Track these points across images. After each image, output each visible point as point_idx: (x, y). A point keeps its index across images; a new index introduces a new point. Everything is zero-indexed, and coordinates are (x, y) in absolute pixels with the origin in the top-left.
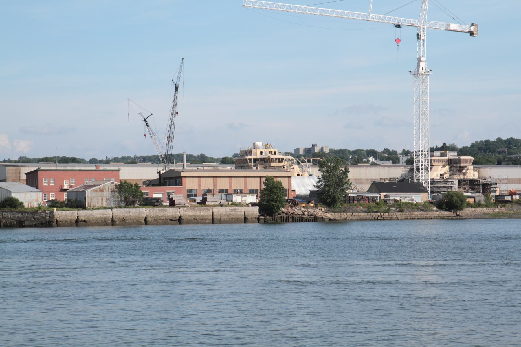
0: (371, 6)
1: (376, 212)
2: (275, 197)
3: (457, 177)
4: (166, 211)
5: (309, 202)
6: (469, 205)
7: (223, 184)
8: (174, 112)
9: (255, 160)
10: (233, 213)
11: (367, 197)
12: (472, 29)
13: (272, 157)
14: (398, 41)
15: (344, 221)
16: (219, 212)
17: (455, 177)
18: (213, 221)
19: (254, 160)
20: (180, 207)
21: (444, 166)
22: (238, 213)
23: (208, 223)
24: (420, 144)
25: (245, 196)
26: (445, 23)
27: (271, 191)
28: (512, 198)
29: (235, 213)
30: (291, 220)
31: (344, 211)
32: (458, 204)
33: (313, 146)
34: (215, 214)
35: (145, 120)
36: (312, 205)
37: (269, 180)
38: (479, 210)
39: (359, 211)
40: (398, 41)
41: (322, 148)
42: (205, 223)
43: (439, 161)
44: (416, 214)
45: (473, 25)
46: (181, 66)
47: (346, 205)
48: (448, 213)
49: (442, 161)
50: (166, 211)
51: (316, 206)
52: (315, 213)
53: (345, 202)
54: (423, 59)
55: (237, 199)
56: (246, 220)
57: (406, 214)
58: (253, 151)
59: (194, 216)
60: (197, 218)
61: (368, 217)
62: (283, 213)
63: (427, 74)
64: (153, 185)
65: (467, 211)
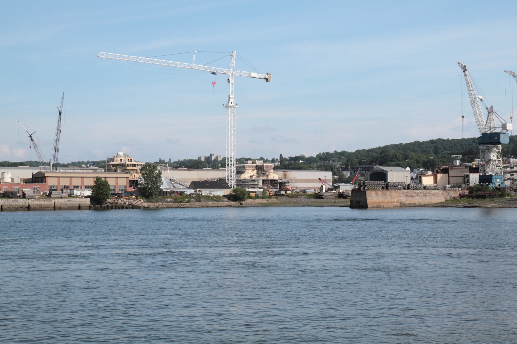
0: (194, 59)
1: (181, 202)
2: (102, 191)
3: (262, 178)
4: (17, 201)
5: (132, 195)
6: (250, 197)
7: (65, 182)
8: (59, 131)
9: (116, 165)
10: (70, 203)
11: (177, 192)
12: (267, 77)
13: (128, 163)
14: (214, 84)
15: (156, 209)
16: (59, 202)
17: (261, 178)
18: (55, 208)
19: (115, 165)
20: (29, 199)
21: (253, 170)
22: (74, 203)
23: (50, 210)
24: (232, 153)
25: (83, 191)
26: (247, 72)
27: (99, 187)
28: (286, 193)
29: (72, 203)
30: (114, 208)
31: (157, 202)
32: (241, 196)
33: (211, 155)
34: (56, 203)
35: (30, 136)
36: (134, 197)
37: (98, 180)
38: (257, 201)
39: (169, 201)
40: (214, 84)
41: (217, 157)
42: (48, 210)
43: (250, 167)
44: (210, 203)
45: (267, 74)
46: (63, 98)
47: (160, 197)
48: (234, 203)
49: (252, 167)
50: (17, 201)
51: (137, 198)
52: (134, 203)
53: (159, 195)
54: (231, 96)
55: (77, 192)
56: (80, 208)
57: (203, 203)
58: (115, 158)
59: (40, 205)
60: (42, 206)
61: (174, 206)
62: (109, 202)
63: (234, 107)
64: (29, 183)
65: (248, 201)
